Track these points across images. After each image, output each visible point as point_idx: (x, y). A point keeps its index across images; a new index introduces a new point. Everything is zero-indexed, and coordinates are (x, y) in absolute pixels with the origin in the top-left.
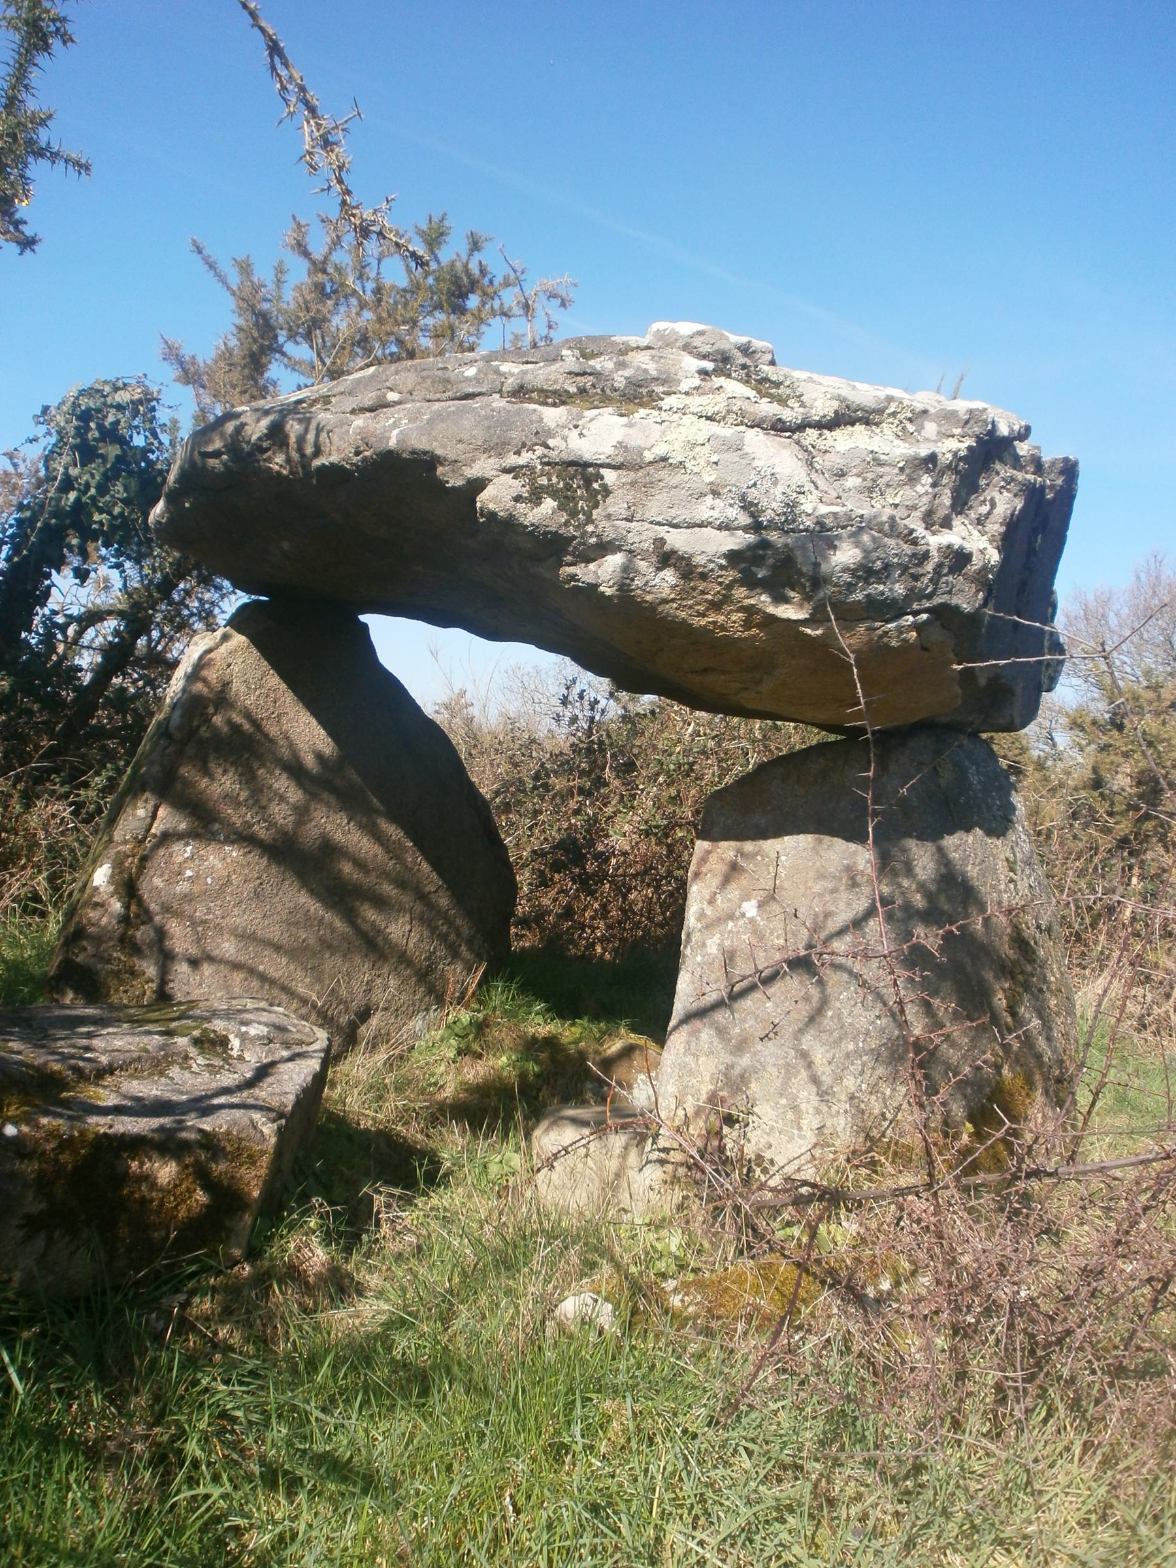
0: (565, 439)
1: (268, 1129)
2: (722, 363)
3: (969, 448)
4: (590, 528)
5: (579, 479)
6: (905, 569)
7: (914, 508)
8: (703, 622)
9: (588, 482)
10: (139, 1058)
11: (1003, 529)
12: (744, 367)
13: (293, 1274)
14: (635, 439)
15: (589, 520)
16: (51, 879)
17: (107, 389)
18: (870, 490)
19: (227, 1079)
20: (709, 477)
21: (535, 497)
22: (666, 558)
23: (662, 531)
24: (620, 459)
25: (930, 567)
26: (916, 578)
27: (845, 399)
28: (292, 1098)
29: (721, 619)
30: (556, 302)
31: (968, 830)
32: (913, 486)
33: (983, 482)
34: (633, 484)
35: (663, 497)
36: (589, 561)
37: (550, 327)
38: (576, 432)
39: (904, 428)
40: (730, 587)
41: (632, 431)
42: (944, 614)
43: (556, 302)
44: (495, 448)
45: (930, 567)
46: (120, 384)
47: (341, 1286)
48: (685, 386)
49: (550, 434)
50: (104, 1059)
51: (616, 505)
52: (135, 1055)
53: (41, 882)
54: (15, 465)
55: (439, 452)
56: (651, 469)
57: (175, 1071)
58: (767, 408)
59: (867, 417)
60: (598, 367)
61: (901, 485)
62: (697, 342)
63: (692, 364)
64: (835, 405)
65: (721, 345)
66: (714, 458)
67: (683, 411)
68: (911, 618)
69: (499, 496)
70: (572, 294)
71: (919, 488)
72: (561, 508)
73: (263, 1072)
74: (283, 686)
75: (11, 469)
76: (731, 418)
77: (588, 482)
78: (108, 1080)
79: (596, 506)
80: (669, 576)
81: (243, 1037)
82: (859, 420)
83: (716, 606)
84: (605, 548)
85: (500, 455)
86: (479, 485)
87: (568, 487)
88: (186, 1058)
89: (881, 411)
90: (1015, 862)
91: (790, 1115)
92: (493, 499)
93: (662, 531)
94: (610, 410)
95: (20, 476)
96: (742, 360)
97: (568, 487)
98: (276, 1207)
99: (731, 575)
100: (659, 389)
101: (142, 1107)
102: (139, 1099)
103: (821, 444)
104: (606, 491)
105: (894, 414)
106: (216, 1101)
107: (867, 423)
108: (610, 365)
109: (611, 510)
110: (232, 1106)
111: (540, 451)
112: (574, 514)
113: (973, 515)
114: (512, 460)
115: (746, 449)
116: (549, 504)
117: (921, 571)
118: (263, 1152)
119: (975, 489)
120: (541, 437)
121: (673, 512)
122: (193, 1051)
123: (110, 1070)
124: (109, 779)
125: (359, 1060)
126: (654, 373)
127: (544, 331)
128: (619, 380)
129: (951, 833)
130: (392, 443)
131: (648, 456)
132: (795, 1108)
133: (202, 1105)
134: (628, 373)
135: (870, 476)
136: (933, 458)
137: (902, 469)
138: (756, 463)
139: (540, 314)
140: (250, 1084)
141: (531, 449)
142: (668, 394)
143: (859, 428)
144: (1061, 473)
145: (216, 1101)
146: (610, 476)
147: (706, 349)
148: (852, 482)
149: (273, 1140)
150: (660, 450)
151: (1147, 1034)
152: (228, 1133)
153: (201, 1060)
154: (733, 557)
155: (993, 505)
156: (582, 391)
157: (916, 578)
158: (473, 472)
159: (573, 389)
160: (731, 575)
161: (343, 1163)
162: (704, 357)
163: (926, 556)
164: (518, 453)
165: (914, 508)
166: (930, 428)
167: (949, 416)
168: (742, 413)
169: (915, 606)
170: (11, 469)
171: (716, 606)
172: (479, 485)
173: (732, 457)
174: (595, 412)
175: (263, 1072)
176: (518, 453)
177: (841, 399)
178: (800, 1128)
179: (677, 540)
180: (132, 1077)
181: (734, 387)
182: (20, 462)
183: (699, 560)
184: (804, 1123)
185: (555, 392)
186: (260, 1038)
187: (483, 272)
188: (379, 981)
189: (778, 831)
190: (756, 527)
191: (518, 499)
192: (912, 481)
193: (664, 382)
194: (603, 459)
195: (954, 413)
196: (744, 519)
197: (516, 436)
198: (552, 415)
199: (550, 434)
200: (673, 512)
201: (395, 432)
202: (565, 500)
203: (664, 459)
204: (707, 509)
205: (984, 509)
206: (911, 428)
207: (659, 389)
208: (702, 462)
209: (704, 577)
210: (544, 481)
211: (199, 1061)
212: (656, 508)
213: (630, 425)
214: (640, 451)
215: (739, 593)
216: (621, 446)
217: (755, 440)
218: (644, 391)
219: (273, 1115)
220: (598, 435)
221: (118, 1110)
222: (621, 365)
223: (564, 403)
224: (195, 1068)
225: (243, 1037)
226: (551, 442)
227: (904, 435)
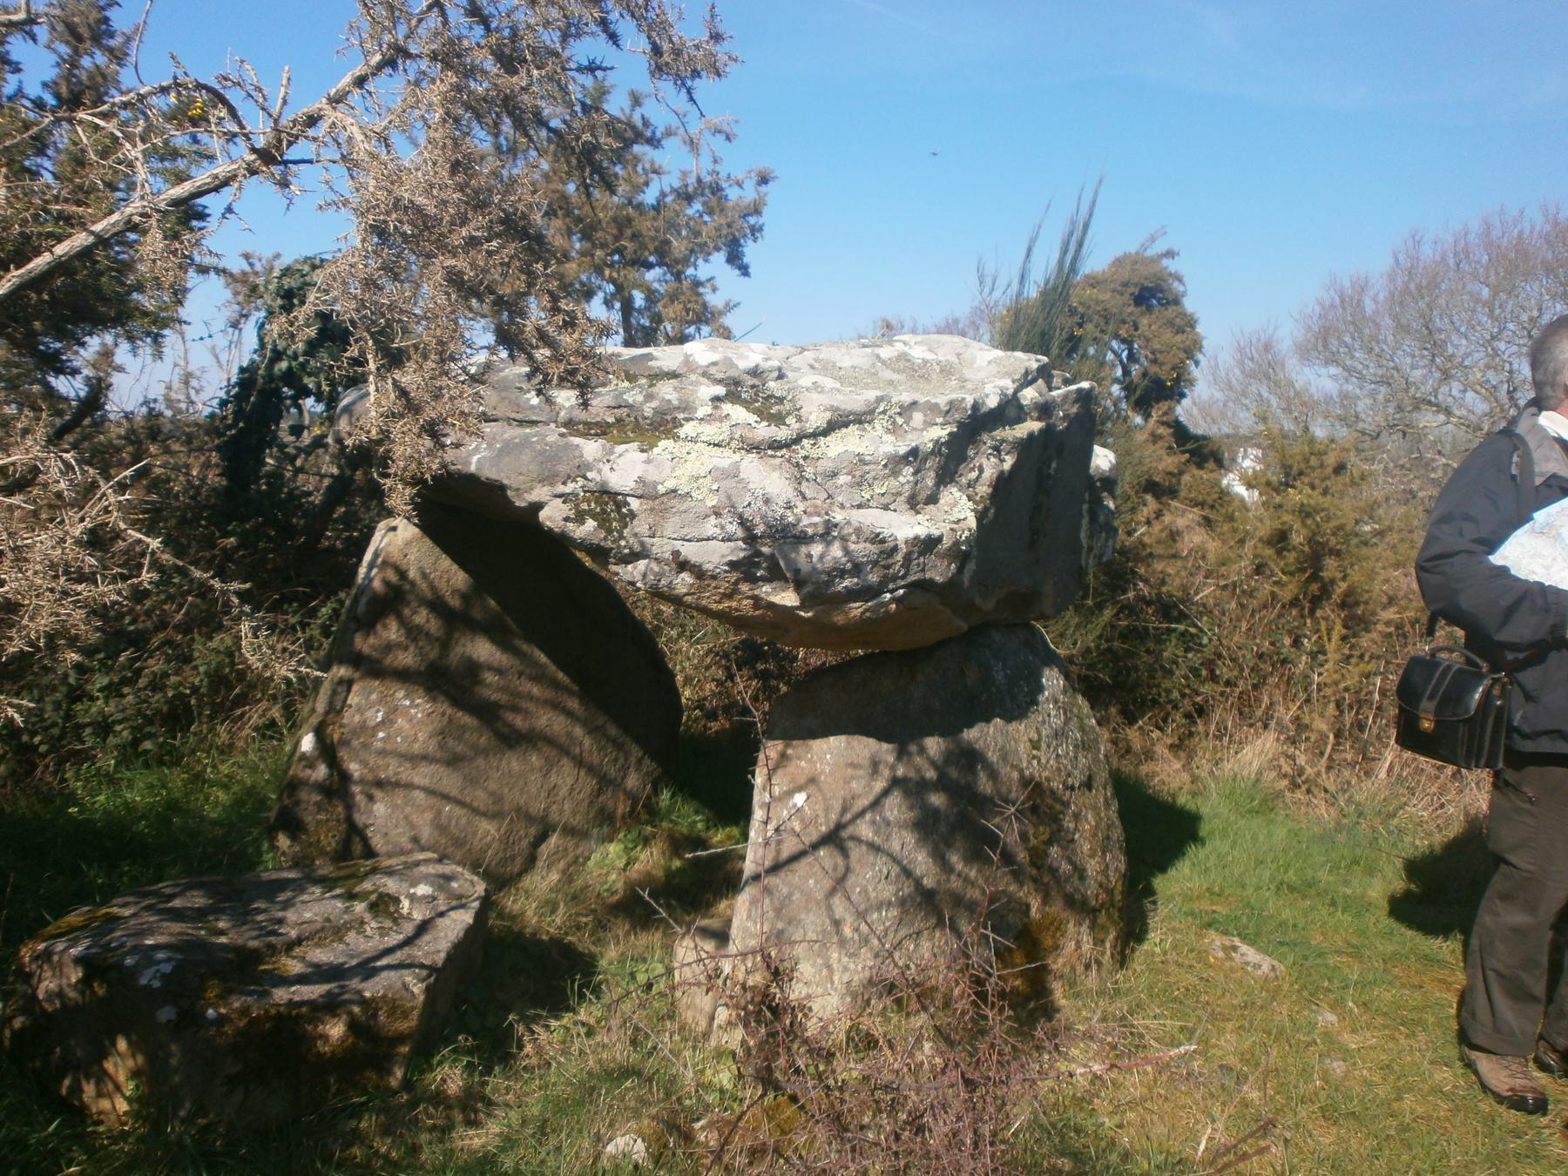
0: (599, 472)
1: (418, 989)
2: (734, 390)
3: (950, 434)
4: (623, 543)
5: (608, 504)
6: (875, 563)
7: (899, 494)
8: (720, 607)
9: (619, 506)
10: (323, 929)
11: (990, 490)
12: (753, 387)
13: (439, 1098)
14: (652, 475)
15: (621, 537)
16: (286, 707)
17: (307, 268)
18: (859, 484)
19: (393, 939)
20: (712, 502)
21: (580, 518)
22: (683, 565)
23: (678, 545)
24: (640, 492)
25: (899, 557)
26: (888, 567)
27: (837, 409)
28: (443, 955)
29: (734, 604)
30: (721, 137)
31: (988, 721)
32: (896, 478)
33: (971, 453)
34: (652, 510)
35: (676, 519)
36: (627, 563)
37: (715, 161)
38: (608, 466)
39: (894, 423)
40: (736, 583)
41: (650, 467)
42: (923, 586)
43: (721, 137)
44: (548, 479)
45: (899, 557)
46: (317, 262)
47: (473, 1105)
48: (700, 413)
49: (589, 467)
50: (293, 934)
51: (641, 526)
52: (319, 926)
53: (276, 713)
54: (251, 265)
55: (505, 482)
56: (664, 499)
57: (351, 937)
58: (764, 431)
59: (861, 419)
60: (631, 401)
61: (885, 477)
62: (713, 370)
63: (709, 390)
64: (828, 415)
65: (732, 373)
66: (715, 487)
67: (694, 440)
68: (888, 596)
69: (553, 515)
70: (736, 129)
71: (901, 479)
72: (600, 526)
73: (423, 927)
74: (455, 567)
75: (248, 269)
76: (734, 444)
77: (619, 506)
78: (297, 951)
79: (626, 526)
80: (686, 577)
81: (412, 898)
82: (854, 422)
83: (729, 596)
84: (634, 557)
85: (552, 485)
86: (538, 506)
87: (604, 511)
88: (362, 923)
89: (872, 412)
90: (1040, 740)
91: (825, 972)
92: (549, 518)
93: (678, 545)
94: (635, 445)
95: (256, 274)
96: (751, 381)
97: (604, 511)
98: (426, 1046)
99: (734, 576)
100: (681, 416)
101: (320, 973)
102: (317, 966)
103: (814, 453)
104: (632, 515)
105: (884, 412)
106: (379, 964)
107: (860, 422)
108: (640, 398)
109: (637, 530)
110: (389, 967)
111: (581, 482)
112: (609, 531)
113: (964, 481)
114: (561, 489)
115: (742, 476)
116: (591, 524)
117: (890, 561)
118: (413, 1008)
119: (963, 458)
120: (582, 469)
121: (685, 531)
122: (367, 917)
123: (299, 941)
124: (334, 610)
125: (537, 878)
126: (676, 403)
127: (710, 167)
128: (648, 410)
129: (970, 725)
130: (473, 468)
131: (661, 489)
132: (829, 967)
133: (367, 969)
134: (655, 404)
135: (858, 473)
136: (914, 452)
137: (885, 466)
138: (751, 486)
139: (704, 151)
140: (408, 942)
141: (574, 480)
142: (687, 420)
143: (853, 428)
144: (1076, 401)
145: (379, 964)
146: (634, 504)
147: (720, 376)
148: (843, 479)
149: (422, 998)
150: (670, 484)
151: (1299, 795)
152: (384, 996)
153: (374, 924)
154: (733, 565)
155: (981, 470)
156: (619, 420)
157: (888, 567)
158: (533, 497)
159: (611, 420)
160: (734, 576)
161: (507, 981)
162: (719, 382)
163: (895, 549)
164: (564, 483)
165: (899, 494)
166: (918, 417)
167: (933, 408)
168: (742, 439)
169: (891, 586)
170: (248, 269)
171: (729, 596)
172: (538, 506)
173: (731, 483)
174: (624, 447)
175: (423, 927)
176: (564, 483)
177: (834, 409)
178: (832, 983)
179: (690, 551)
180: (317, 945)
181: (738, 413)
182: (256, 262)
183: (706, 567)
184: (836, 978)
185: (597, 424)
186: (424, 897)
187: (646, 123)
188: (554, 807)
189: (825, 733)
190: (751, 539)
191: (567, 519)
192: (895, 473)
193: (684, 410)
194: (627, 490)
195: (937, 405)
196: (740, 533)
197: (563, 469)
198: (591, 448)
199: (589, 467)
200: (685, 531)
201: (475, 459)
202: (603, 520)
203: (674, 491)
204: (710, 527)
205: (974, 475)
206: (900, 421)
207: (681, 416)
208: (705, 491)
209: (714, 577)
210: (585, 506)
211: (372, 925)
212: (671, 527)
213: (648, 462)
214: (655, 484)
215: (744, 587)
216: (640, 481)
217: (751, 465)
218: (669, 418)
219: (425, 973)
220: (625, 468)
221: (302, 979)
222: (649, 397)
223: (604, 433)
224: (369, 932)
225: (412, 898)
226: (590, 475)
227: (894, 430)
